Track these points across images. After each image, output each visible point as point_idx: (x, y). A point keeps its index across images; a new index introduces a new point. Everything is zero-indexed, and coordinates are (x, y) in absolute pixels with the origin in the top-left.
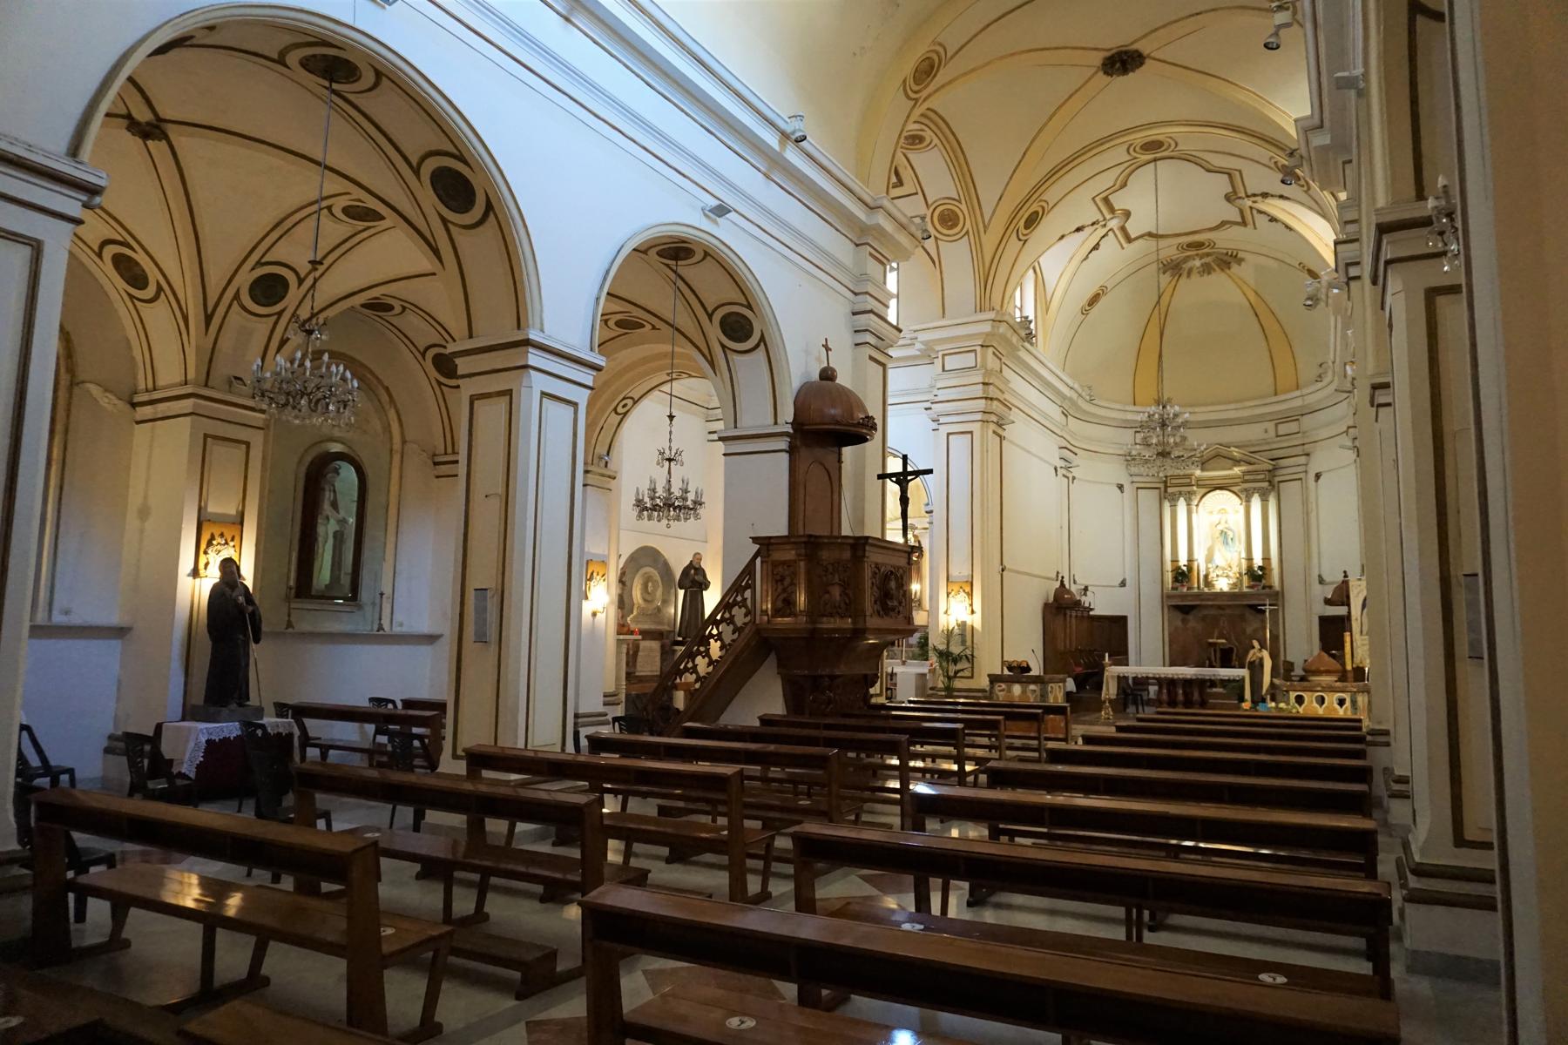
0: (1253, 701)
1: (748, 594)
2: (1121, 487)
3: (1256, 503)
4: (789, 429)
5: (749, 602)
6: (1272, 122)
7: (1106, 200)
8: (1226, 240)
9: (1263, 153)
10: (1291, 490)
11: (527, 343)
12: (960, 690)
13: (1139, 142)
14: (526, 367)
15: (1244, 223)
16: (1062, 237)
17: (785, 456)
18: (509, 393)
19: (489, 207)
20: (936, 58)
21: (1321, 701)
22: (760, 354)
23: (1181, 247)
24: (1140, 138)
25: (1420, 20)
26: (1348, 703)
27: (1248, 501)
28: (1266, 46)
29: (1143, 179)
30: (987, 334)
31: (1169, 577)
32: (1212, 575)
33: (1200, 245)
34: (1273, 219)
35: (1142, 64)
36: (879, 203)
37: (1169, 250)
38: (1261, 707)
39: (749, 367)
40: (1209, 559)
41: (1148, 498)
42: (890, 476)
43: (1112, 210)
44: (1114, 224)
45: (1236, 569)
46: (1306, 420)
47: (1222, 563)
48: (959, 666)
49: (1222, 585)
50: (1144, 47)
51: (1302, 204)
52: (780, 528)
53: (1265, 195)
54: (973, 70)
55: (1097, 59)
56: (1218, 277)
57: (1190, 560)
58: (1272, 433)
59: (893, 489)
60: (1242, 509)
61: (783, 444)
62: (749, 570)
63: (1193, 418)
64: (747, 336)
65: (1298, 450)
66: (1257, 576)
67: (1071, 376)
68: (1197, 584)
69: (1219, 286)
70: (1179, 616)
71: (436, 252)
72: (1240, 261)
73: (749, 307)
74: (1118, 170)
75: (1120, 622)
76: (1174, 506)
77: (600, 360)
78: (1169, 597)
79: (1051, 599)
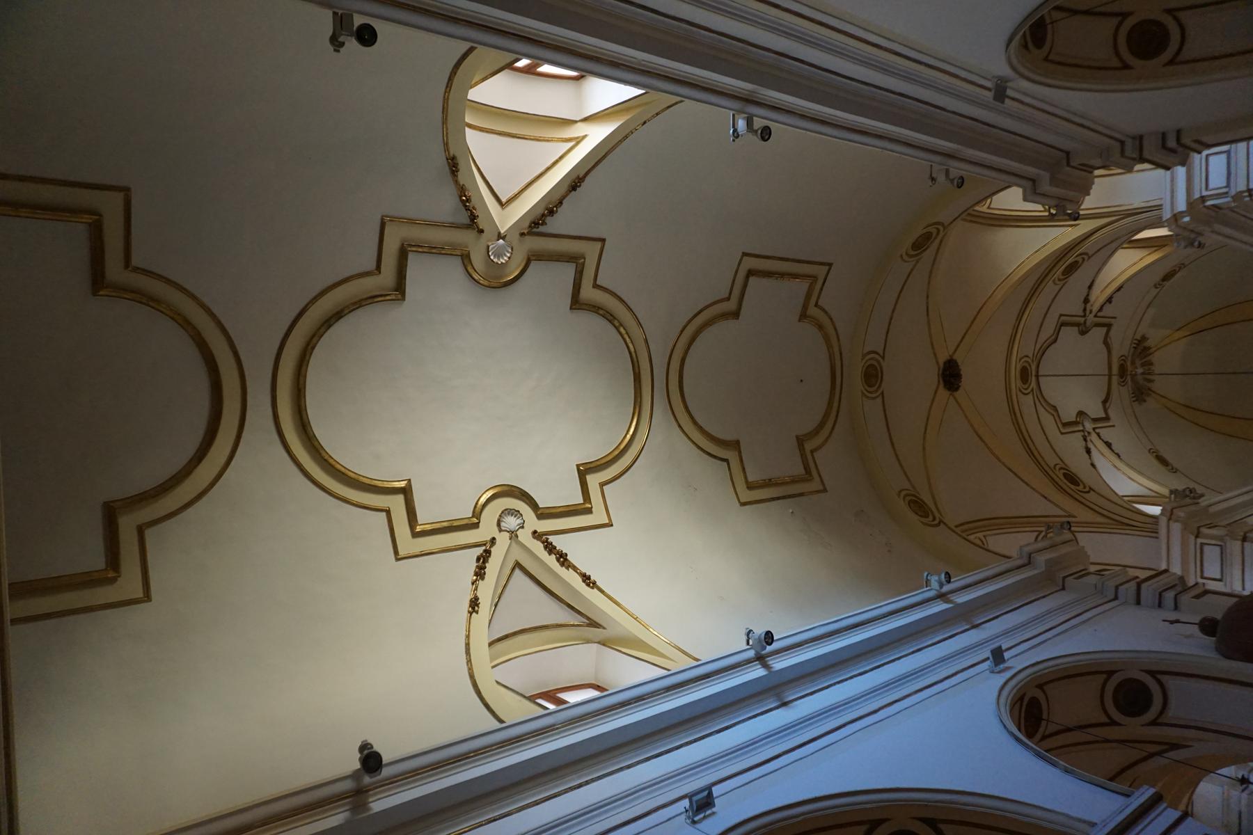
7: (1065, 425)
8: (1122, 345)
9: (1050, 288)
13: (1019, 383)
15: (1109, 326)
16: (1093, 465)
20: (908, 498)
22: (1172, 683)
23: (1123, 383)
24: (1015, 383)
28: (959, 187)
29: (1054, 390)
33: (1123, 371)
34: (1109, 300)
37: (1122, 394)
39: (1187, 701)
44: (1089, 426)
50: (943, 358)
51: (1105, 263)
53: (1086, 301)
55: (943, 393)
56: (1156, 358)
69: (1168, 359)
72: (1144, 338)
73: (1110, 673)
77: (1145, 794)
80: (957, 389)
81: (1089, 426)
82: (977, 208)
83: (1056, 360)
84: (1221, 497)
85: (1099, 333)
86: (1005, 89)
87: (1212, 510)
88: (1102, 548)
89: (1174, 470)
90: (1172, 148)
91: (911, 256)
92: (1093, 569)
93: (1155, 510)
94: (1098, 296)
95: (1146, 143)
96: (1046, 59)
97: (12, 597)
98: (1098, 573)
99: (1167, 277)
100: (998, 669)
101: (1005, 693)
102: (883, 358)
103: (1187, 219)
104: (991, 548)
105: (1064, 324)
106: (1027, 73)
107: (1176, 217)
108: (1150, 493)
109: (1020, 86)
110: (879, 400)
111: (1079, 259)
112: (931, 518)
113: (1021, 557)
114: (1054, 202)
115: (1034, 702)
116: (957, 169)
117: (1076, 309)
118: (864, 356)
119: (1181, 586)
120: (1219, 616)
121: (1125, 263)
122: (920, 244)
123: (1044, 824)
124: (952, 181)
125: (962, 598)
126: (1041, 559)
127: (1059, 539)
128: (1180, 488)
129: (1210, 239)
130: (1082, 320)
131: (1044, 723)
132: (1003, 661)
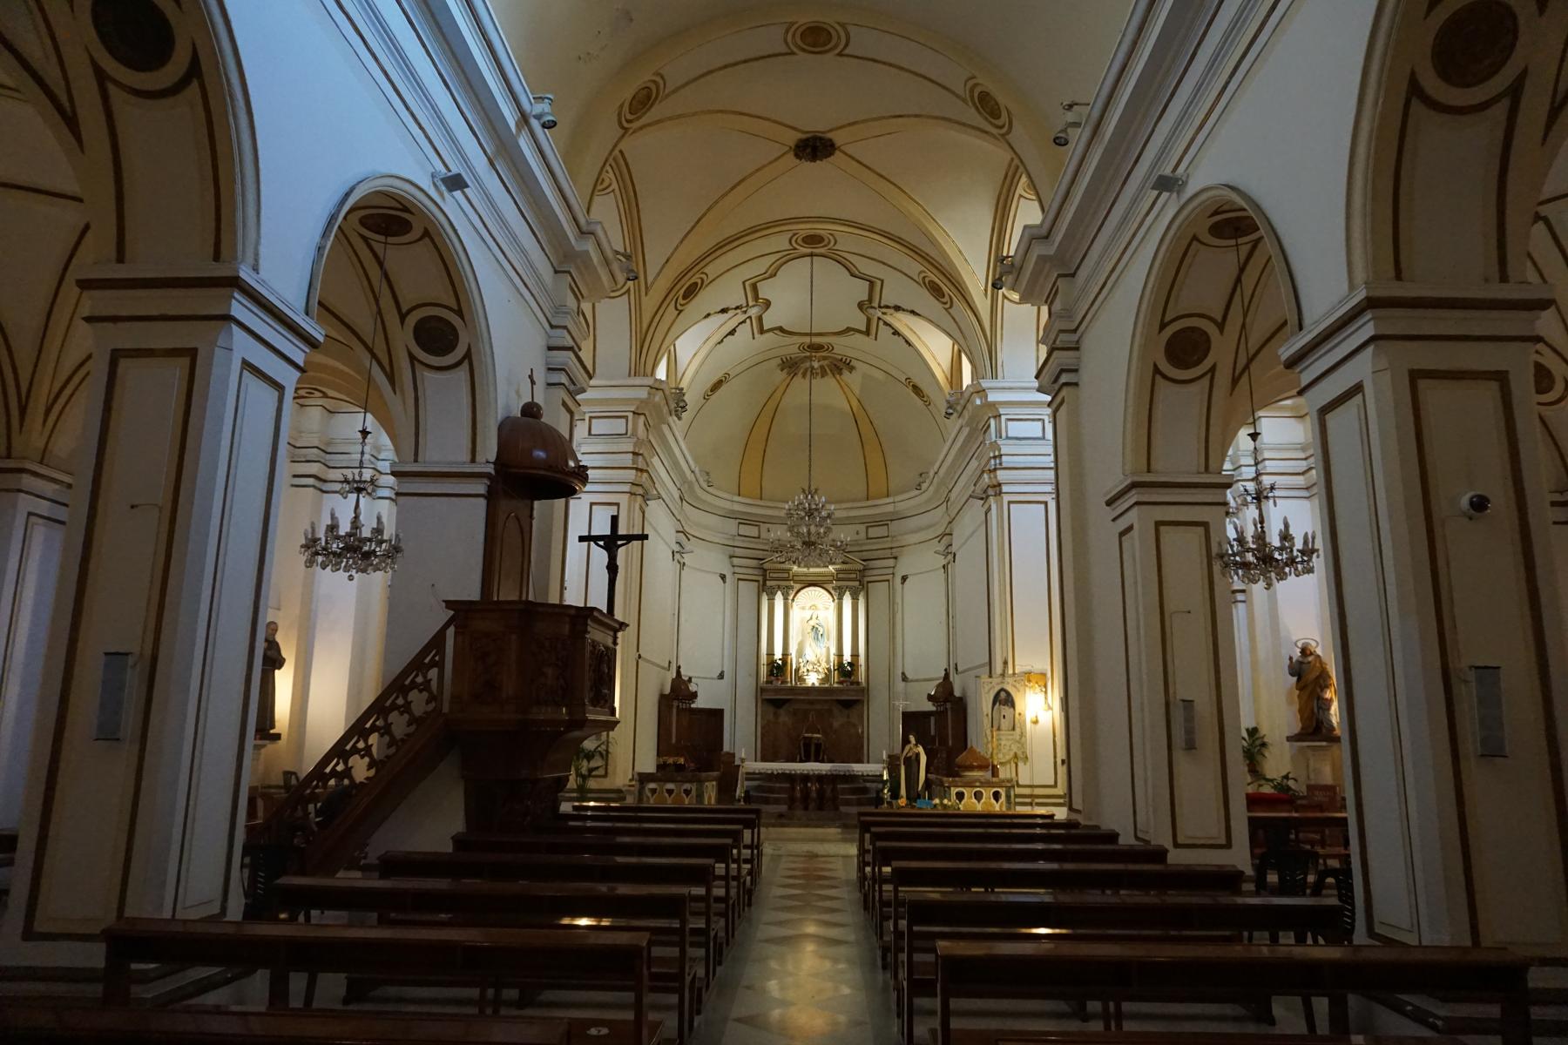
0: (908, 798)
1: (433, 673)
2: (723, 577)
3: (847, 601)
4: (490, 469)
5: (434, 685)
6: (934, 242)
7: (754, 288)
9: (915, 267)
10: (879, 590)
11: (235, 283)
12: (592, 791)
13: (803, 233)
14: (228, 318)
15: (867, 333)
17: (482, 502)
18: (192, 353)
19: (194, 70)
21: (978, 796)
22: (462, 374)
23: (802, 347)
24: (805, 229)
25: (1415, 103)
26: (1003, 798)
27: (841, 599)
30: (642, 401)
31: (764, 670)
32: (803, 669)
33: (819, 348)
34: (896, 333)
35: (831, 154)
36: (592, 228)
37: (791, 347)
38: (919, 804)
39: (444, 391)
40: (800, 653)
41: (748, 590)
42: (595, 539)
43: (756, 298)
44: (753, 312)
45: (824, 665)
46: (894, 526)
47: (812, 658)
48: (593, 764)
49: (812, 680)
50: (838, 138)
51: (938, 326)
52: (473, 593)
53: (897, 308)
54: (679, 116)
55: (792, 138)
56: (830, 382)
57: (785, 654)
58: (863, 535)
59: (600, 556)
60: (832, 606)
61: (480, 487)
62: (437, 641)
63: (838, 514)
64: (450, 347)
65: (887, 553)
66: (846, 672)
67: (696, 459)
68: (791, 681)
69: (828, 391)
70: (771, 709)
71: (71, 121)
72: (851, 369)
73: (460, 313)
74: (773, 258)
75: (717, 714)
76: (771, 600)
78: (763, 690)
79: (667, 691)
80: (797, 156)
81: (753, 312)
82: (1024, 179)
83: (830, 277)
84: (680, 439)
85: (859, 321)
86: (1170, 190)
87: (665, 428)
88: (612, 323)
89: (706, 397)
90: (1059, 378)
91: (972, 91)
92: (586, 307)
93: (661, 373)
94: (902, 321)
95: (1071, 353)
96: (1195, 238)
97: (721, 711)
98: (580, 312)
99: (917, 390)
100: (440, 183)
101: (407, 187)
102: (840, 54)
103: (978, 402)
104: (596, 199)
105: (872, 284)
106: (1185, 212)
107: (982, 392)
108: (680, 370)
109: (1170, 206)
110: (784, 49)
111: (946, 299)
112: (629, 117)
113: (588, 223)
114: (1017, 264)
115: (405, 227)
116: (1078, 137)
117: (889, 298)
118: (843, 25)
119: (574, 389)
120: (545, 419)
121: (936, 348)
122: (987, 105)
123: (239, 214)
124: (1064, 131)
125: (524, 144)
126: (589, 246)
127: (615, 267)
128: (686, 398)
129: (954, 424)
130: (876, 304)
131: (382, 238)
132: (450, 190)
